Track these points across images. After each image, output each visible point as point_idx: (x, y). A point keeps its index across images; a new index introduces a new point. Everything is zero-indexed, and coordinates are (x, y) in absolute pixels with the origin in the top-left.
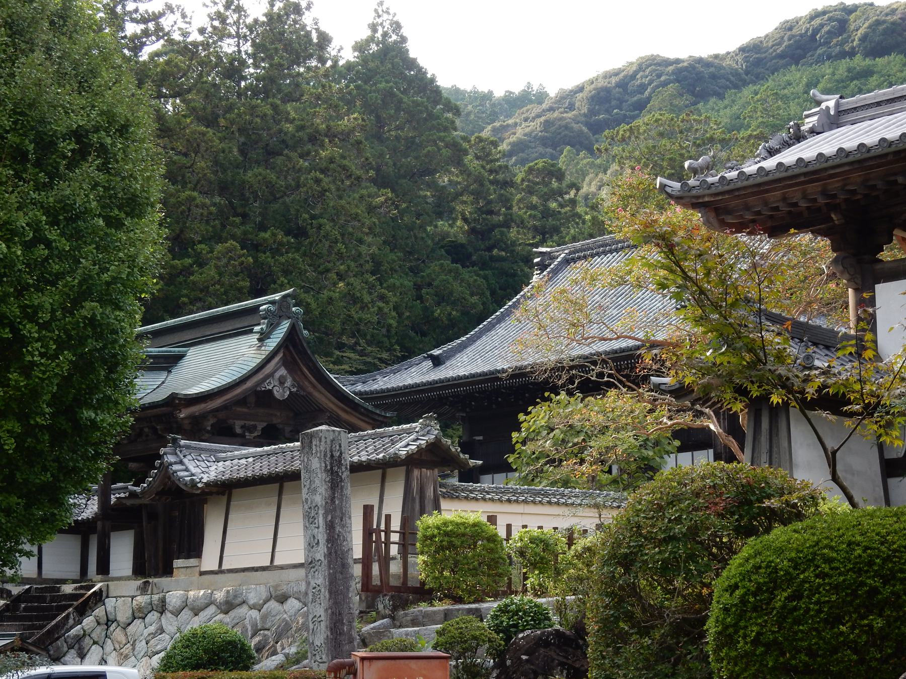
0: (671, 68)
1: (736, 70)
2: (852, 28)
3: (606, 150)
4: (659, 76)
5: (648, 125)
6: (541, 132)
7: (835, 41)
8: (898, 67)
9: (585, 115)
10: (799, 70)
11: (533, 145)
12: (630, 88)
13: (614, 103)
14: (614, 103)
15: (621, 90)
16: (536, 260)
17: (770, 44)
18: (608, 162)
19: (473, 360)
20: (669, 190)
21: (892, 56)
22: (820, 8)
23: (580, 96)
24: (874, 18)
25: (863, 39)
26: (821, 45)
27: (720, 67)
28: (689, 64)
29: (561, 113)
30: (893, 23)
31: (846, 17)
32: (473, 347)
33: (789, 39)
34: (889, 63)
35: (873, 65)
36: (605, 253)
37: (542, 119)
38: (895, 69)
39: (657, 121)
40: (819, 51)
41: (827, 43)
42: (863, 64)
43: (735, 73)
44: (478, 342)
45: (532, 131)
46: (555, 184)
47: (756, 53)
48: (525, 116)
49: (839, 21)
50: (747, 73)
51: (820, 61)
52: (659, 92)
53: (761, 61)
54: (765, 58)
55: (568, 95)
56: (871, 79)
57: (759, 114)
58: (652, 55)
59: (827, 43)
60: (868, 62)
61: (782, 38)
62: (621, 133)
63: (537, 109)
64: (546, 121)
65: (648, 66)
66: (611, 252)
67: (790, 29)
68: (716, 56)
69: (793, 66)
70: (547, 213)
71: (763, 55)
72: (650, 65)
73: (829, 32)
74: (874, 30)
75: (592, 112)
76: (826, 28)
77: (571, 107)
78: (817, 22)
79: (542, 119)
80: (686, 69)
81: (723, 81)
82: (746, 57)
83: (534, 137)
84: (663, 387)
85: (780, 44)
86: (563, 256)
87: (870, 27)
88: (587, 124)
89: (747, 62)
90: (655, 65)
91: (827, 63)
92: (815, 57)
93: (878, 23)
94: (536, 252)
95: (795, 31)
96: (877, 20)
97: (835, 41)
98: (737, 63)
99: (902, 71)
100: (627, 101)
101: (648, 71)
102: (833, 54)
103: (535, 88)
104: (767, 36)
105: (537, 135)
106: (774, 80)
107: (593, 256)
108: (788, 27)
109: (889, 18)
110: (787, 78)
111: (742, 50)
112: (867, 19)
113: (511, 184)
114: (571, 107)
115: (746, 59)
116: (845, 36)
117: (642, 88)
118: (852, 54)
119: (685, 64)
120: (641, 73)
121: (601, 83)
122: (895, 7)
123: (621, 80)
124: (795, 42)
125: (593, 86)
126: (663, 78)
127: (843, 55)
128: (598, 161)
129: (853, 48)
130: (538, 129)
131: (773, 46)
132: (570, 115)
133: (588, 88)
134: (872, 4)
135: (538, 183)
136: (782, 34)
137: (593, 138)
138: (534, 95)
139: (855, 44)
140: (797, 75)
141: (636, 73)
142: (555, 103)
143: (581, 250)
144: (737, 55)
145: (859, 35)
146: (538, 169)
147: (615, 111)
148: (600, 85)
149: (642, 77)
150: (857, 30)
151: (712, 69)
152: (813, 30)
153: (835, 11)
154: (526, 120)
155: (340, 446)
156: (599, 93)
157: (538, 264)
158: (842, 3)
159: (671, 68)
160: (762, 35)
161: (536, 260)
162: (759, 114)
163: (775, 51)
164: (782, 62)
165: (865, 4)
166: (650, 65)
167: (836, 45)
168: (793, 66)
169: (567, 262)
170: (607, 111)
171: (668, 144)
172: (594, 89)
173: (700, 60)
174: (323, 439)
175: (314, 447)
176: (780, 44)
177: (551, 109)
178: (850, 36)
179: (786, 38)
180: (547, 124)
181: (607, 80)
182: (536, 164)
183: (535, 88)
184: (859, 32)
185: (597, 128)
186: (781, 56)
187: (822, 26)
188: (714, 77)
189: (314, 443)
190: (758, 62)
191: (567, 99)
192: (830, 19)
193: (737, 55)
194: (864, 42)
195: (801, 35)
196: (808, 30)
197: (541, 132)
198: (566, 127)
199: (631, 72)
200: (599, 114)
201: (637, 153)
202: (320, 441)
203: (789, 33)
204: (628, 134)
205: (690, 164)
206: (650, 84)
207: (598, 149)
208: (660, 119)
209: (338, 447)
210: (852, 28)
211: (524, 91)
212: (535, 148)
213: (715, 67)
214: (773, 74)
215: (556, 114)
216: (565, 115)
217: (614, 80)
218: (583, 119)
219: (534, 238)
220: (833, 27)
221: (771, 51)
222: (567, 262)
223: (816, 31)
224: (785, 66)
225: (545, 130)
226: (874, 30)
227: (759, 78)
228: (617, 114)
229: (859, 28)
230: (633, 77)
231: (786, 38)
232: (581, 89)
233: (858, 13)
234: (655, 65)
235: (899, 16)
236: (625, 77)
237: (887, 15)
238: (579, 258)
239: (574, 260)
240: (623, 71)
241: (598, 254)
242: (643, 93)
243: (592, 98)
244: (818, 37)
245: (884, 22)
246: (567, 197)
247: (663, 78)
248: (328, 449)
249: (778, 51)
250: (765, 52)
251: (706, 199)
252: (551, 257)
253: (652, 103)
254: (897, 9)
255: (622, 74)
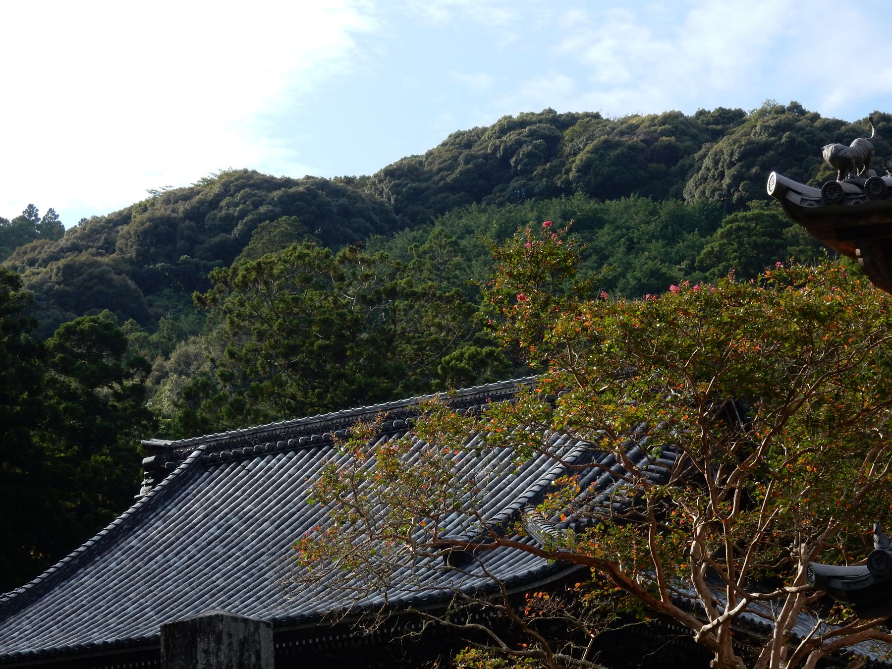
0: (276, 194)
1: (382, 204)
2: (567, 150)
3: (214, 300)
4: (256, 205)
5: (285, 262)
6: (59, 283)
7: (539, 169)
8: (641, 216)
9: (131, 261)
10: (484, 211)
11: (43, 304)
12: (208, 222)
13: (180, 244)
14: (180, 244)
15: (193, 224)
16: (146, 460)
17: (435, 167)
18: (170, 339)
19: (39, 630)
20: (795, 199)
21: (632, 198)
22: (515, 115)
23: (123, 229)
24: (602, 138)
25: (585, 168)
26: (516, 174)
27: (356, 198)
28: (308, 189)
29: (93, 255)
30: (632, 148)
31: (558, 132)
32: (38, 606)
33: (467, 162)
34: (627, 208)
35: (602, 210)
36: (273, 452)
37: (61, 263)
38: (637, 219)
39: (301, 257)
40: (514, 184)
41: (526, 172)
42: (587, 207)
43: (380, 209)
44: (47, 599)
45: (42, 283)
46: (108, 361)
47: (413, 181)
48: (30, 256)
49: (546, 136)
50: (397, 211)
51: (516, 199)
52: (264, 228)
53: (420, 192)
54: (428, 188)
55: (103, 227)
56: (600, 232)
57: (426, 274)
58: (246, 171)
59: (526, 172)
60: (593, 205)
61: (455, 158)
62: (241, 273)
63: (51, 248)
64: (68, 267)
65: (239, 189)
66: (284, 450)
67: (468, 145)
68: (349, 181)
69: (474, 204)
70: (96, 406)
71: (424, 185)
72: (243, 187)
73: (529, 155)
74: (602, 157)
75: (144, 257)
76: (526, 149)
77: (109, 247)
78: (511, 137)
79: (61, 263)
80: (300, 196)
81: (361, 220)
82: (396, 186)
83: (47, 292)
84: (837, 584)
85: (451, 168)
86: (194, 454)
87: (595, 151)
88: (134, 276)
89: (398, 193)
90: (251, 186)
91: (528, 203)
92: (507, 193)
93: (608, 145)
94: (146, 447)
95: (475, 150)
96: (606, 141)
97: (539, 169)
98: (381, 193)
99: (648, 223)
100: (204, 242)
101: (239, 196)
102: (537, 190)
103: (41, 214)
104: (430, 154)
105: (51, 288)
106: (443, 224)
107: (250, 456)
108: (463, 142)
109: (625, 138)
110: (464, 221)
111: (390, 173)
112: (591, 138)
113: (42, 353)
114: (109, 247)
115: (396, 189)
116: (555, 162)
117: (229, 223)
118: (568, 190)
119: (301, 189)
120: (227, 199)
121: (161, 211)
122: (634, 121)
123: (193, 208)
124: (476, 166)
125: (146, 215)
126: (262, 209)
127: (553, 192)
128: (154, 337)
129: (568, 182)
130: (54, 279)
131: (440, 170)
132: (105, 260)
133: (137, 218)
134: (597, 116)
135: (81, 356)
136: (455, 152)
137: (144, 300)
138: (39, 227)
139: (571, 175)
140: (484, 220)
141: (219, 198)
142: (81, 238)
143: (228, 445)
144: (381, 181)
145: (578, 162)
146: (82, 331)
147: (183, 257)
148: (158, 214)
149: (228, 206)
150: (575, 154)
151: (343, 201)
152: (505, 149)
153: (540, 121)
154: (32, 263)
155: (258, 657)
156: (156, 226)
157: (148, 466)
158: (551, 111)
159: (276, 194)
160: (422, 152)
161: (146, 460)
162: (426, 274)
163: (442, 178)
164: (453, 197)
165: (587, 115)
166: (243, 187)
167: (541, 176)
168: (474, 204)
169: (202, 465)
170: (169, 258)
171: (316, 298)
172: (149, 220)
173: (323, 184)
174: (225, 639)
175: (200, 656)
176: (451, 168)
177: (75, 248)
178: (563, 164)
179: (461, 159)
180: (69, 271)
181: (171, 206)
182: (79, 323)
183: (41, 214)
184: (578, 157)
185: (150, 283)
186: (452, 188)
187: (519, 143)
188: (345, 213)
189: (201, 646)
190: (416, 195)
191: (101, 232)
192: (532, 134)
193: (381, 181)
194: (585, 174)
195: (486, 157)
196: (496, 148)
197: (59, 283)
198: (102, 278)
199: (211, 196)
200: (155, 261)
201: (265, 310)
202: (219, 641)
203: (466, 152)
204: (254, 275)
205: (837, 150)
206: (242, 215)
207: (199, 298)
208: (307, 255)
209: (253, 659)
210: (567, 150)
211: (21, 218)
212: (47, 309)
213: (349, 197)
214: (443, 214)
215: (84, 257)
216: (99, 259)
217: (182, 207)
218: (129, 268)
219: (68, 447)
220: (536, 147)
221: (436, 178)
222: (202, 465)
223: (510, 151)
224: (460, 203)
225: (65, 282)
226: (602, 157)
227: (416, 220)
228: (185, 262)
229: (579, 153)
230: (214, 203)
231: (461, 159)
232: (124, 218)
233: (576, 127)
234: (251, 186)
235: (641, 137)
236: (201, 203)
237: (622, 133)
238: (227, 460)
239: (216, 463)
240: (198, 193)
241: (261, 454)
242: (229, 231)
243: (146, 233)
244: (512, 161)
245: (618, 144)
246: (128, 383)
247: (262, 209)
248: (235, 660)
249: (449, 180)
250: (427, 180)
251: (875, 220)
252: (172, 456)
253: (251, 245)
254: (637, 126)
255: (197, 198)
